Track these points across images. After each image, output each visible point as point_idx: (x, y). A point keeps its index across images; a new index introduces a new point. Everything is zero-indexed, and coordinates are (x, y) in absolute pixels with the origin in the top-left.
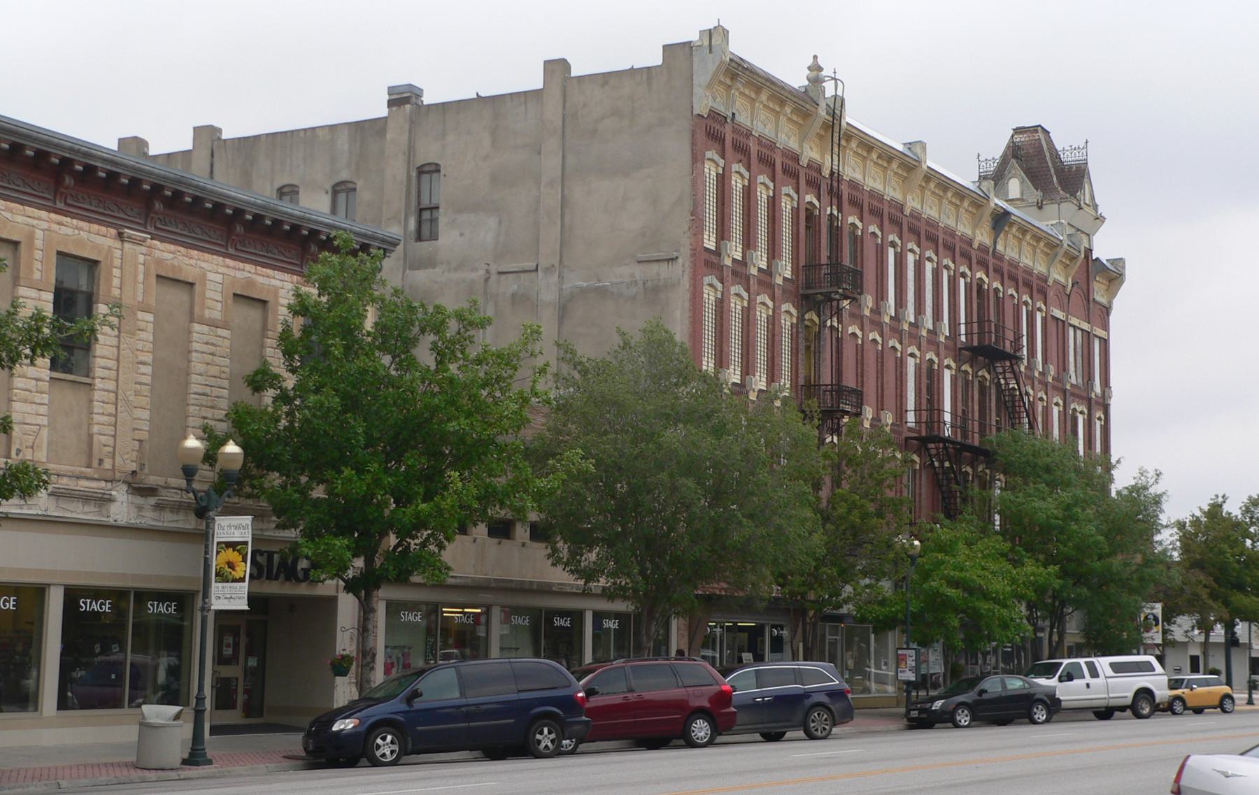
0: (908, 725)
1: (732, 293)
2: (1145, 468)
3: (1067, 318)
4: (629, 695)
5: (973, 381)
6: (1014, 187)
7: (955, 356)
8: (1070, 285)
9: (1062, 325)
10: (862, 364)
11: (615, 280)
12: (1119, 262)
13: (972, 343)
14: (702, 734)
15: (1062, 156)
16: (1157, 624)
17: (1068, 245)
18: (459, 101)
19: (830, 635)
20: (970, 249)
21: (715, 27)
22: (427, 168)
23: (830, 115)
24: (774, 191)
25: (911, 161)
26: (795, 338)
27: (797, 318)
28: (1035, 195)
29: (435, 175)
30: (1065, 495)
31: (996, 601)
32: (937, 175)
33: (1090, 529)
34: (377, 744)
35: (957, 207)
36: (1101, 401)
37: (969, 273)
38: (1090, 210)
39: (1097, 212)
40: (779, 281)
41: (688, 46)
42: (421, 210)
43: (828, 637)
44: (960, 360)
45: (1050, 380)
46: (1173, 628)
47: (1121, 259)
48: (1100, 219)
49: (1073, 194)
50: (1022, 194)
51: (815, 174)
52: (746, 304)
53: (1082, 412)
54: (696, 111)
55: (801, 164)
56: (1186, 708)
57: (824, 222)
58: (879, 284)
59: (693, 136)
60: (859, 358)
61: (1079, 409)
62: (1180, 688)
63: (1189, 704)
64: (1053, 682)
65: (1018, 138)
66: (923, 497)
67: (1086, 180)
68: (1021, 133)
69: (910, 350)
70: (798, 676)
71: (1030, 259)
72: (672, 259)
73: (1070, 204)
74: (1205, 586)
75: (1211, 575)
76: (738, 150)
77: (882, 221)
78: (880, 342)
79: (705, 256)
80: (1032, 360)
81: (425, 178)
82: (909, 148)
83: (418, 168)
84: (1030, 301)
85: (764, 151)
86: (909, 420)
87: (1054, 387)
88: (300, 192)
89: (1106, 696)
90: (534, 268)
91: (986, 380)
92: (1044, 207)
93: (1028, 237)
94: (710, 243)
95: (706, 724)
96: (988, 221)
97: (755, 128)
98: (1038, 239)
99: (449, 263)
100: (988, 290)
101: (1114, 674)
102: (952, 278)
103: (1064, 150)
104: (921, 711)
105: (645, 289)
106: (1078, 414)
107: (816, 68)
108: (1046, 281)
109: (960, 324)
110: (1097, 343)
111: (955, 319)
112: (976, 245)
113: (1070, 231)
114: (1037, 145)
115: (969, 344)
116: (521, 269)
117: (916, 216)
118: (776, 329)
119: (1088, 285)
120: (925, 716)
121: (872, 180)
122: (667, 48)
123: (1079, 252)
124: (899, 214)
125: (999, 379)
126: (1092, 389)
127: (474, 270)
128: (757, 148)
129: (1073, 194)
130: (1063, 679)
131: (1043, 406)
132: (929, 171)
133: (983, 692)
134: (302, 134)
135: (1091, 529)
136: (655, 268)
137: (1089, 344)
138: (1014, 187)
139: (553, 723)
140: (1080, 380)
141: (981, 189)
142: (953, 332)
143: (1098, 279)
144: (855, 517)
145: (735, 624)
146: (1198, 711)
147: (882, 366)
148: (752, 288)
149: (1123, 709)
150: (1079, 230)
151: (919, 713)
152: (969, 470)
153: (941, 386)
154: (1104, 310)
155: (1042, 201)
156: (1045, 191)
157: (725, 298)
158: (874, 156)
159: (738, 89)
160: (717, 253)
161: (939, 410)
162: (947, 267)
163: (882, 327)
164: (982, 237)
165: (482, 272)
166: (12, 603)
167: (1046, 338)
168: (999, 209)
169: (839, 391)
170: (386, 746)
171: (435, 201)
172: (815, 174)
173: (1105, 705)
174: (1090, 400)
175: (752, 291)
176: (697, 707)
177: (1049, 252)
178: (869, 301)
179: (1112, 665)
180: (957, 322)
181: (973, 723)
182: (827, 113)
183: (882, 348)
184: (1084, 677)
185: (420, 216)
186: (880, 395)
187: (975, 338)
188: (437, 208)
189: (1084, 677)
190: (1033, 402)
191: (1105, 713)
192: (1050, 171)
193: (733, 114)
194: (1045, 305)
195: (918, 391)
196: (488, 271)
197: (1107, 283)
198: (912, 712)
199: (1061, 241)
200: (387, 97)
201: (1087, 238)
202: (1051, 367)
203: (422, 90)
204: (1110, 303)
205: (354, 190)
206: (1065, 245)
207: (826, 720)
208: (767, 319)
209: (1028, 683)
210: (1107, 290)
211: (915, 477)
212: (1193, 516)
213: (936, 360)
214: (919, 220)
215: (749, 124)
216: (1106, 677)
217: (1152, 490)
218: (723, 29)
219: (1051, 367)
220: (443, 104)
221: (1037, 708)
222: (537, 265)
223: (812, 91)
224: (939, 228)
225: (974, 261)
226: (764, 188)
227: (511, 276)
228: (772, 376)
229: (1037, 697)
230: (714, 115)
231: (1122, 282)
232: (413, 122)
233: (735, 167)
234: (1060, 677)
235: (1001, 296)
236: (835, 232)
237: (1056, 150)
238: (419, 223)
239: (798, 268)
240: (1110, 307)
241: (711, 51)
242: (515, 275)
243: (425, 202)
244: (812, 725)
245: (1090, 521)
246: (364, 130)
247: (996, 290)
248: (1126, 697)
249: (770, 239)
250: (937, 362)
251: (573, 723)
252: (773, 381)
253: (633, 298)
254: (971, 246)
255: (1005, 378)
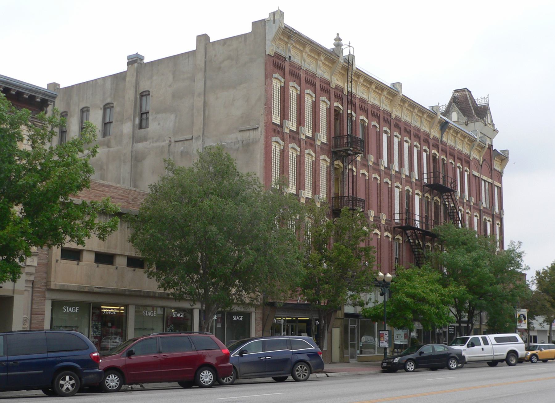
0: (382, 371)
1: (290, 147)
2: (514, 240)
3: (480, 176)
4: (158, 355)
5: (431, 202)
6: (454, 116)
7: (421, 189)
8: (482, 160)
9: (478, 179)
10: (369, 189)
11: (228, 141)
12: (506, 151)
13: (430, 182)
14: (208, 379)
15: (477, 102)
16: (525, 319)
17: (479, 141)
18: (159, 60)
19: (351, 325)
20: (428, 138)
21: (277, 11)
22: (144, 94)
23: (346, 63)
24: (315, 98)
25: (394, 91)
26: (329, 173)
27: (330, 163)
28: (464, 119)
29: (148, 97)
30: (474, 254)
31: (432, 305)
32: (409, 100)
33: (486, 268)
34: (61, 384)
35: (421, 117)
36: (499, 216)
37: (428, 150)
38: (491, 126)
39: (494, 127)
40: (318, 143)
41: (263, 21)
42: (142, 114)
43: (350, 326)
44: (424, 191)
45: (472, 204)
46: (533, 321)
47: (507, 150)
48: (496, 131)
49: (483, 119)
50: (458, 119)
51: (340, 93)
52: (298, 153)
53: (489, 221)
54: (267, 53)
55: (331, 86)
56: (538, 360)
57: (345, 116)
58: (378, 151)
59: (266, 65)
60: (367, 186)
61: (488, 219)
62: (535, 350)
63: (540, 358)
64: (465, 347)
65: (456, 95)
66: (404, 257)
67: (488, 112)
68: (457, 92)
69: (396, 184)
70: (289, 344)
71: (460, 146)
72: (256, 129)
73: (481, 123)
74: (548, 301)
75: (551, 296)
76: (294, 76)
77: (379, 120)
78: (379, 179)
79: (274, 127)
80: (463, 194)
81: (144, 98)
82: (393, 86)
83: (140, 94)
84: (461, 166)
85: (309, 77)
86: (396, 218)
87: (474, 208)
88: (90, 111)
89: (493, 354)
90: (191, 138)
91: (438, 202)
92: (469, 124)
93: (459, 135)
94: (276, 120)
95: (210, 373)
96: (437, 126)
97: (303, 65)
98: (465, 137)
99: (153, 138)
100: (439, 159)
101: (496, 343)
102: (419, 152)
103: (478, 99)
104: (388, 363)
105: (243, 145)
106: (487, 221)
107: (338, 39)
108: (469, 158)
109: (423, 174)
110: (496, 189)
111: (421, 172)
112: (431, 137)
113: (480, 135)
114: (465, 97)
115: (429, 183)
116: (185, 139)
117: (398, 119)
118: (317, 168)
119: (491, 161)
120: (389, 366)
121: (373, 99)
122: (254, 24)
123: (485, 145)
124: (389, 118)
125: (445, 202)
126: (494, 210)
127: (164, 141)
128: (305, 76)
129: (483, 119)
130: (469, 346)
131: (469, 217)
132: (404, 97)
133: (421, 353)
134: (91, 83)
135: (486, 270)
136: (247, 134)
137: (492, 189)
138: (454, 116)
139: (73, 373)
140: (488, 206)
141: (433, 110)
142: (420, 178)
143: (496, 159)
144: (343, 258)
145: (297, 318)
146: (545, 361)
147: (380, 191)
148: (302, 146)
149: (502, 361)
150: (485, 135)
151: (387, 364)
152: (430, 245)
153: (413, 203)
154: (499, 174)
155: (467, 122)
156: (468, 117)
157: (285, 149)
158: (373, 87)
159: (292, 44)
160: (281, 126)
161: (413, 214)
162: (416, 146)
163: (380, 172)
164: (435, 133)
165: (167, 142)
166: (77, 310)
167: (470, 185)
168: (443, 120)
169: (355, 201)
170: (411, 367)
171: (147, 109)
172: (340, 93)
173: (492, 359)
174: (493, 215)
175: (302, 147)
176: (207, 362)
177: (470, 144)
178: (372, 158)
179: (496, 339)
180: (422, 173)
181: (416, 370)
182: (344, 62)
183: (380, 182)
184: (480, 345)
185: (141, 117)
186: (379, 206)
187: (432, 179)
188: (148, 112)
189: (480, 345)
190: (464, 214)
191: (493, 363)
192: (471, 108)
193: (290, 57)
194: (469, 169)
195: (401, 205)
196: (170, 141)
197: (501, 161)
198: (384, 364)
199: (476, 139)
200: (127, 61)
201: (490, 140)
202: (473, 198)
203: (144, 57)
204: (502, 171)
205: (113, 107)
206: (478, 141)
207: (306, 370)
208: (312, 162)
209: (447, 348)
210: (500, 165)
211: (400, 247)
212: (544, 269)
213: (411, 190)
214: (400, 122)
215: (300, 63)
216: (492, 345)
217: (517, 251)
218: (280, 11)
219: (473, 198)
220: (152, 62)
221: (452, 361)
222: (192, 137)
223: (336, 50)
224: (412, 127)
225: (431, 145)
226: (310, 96)
227: (180, 143)
228: (315, 190)
229: (451, 355)
230: (277, 55)
231: (508, 161)
232: (138, 72)
233: (291, 84)
234: (468, 345)
235: (446, 163)
236: (353, 124)
237: (474, 100)
238: (141, 121)
239: (330, 139)
240: (502, 172)
241: (274, 23)
242: (182, 142)
243: (144, 110)
244: (297, 373)
245: (486, 266)
246: (118, 78)
247: (443, 160)
248: (503, 355)
249: (313, 122)
250: (411, 191)
251: (88, 374)
252: (315, 194)
253: (237, 150)
254: (429, 137)
255: (448, 202)
